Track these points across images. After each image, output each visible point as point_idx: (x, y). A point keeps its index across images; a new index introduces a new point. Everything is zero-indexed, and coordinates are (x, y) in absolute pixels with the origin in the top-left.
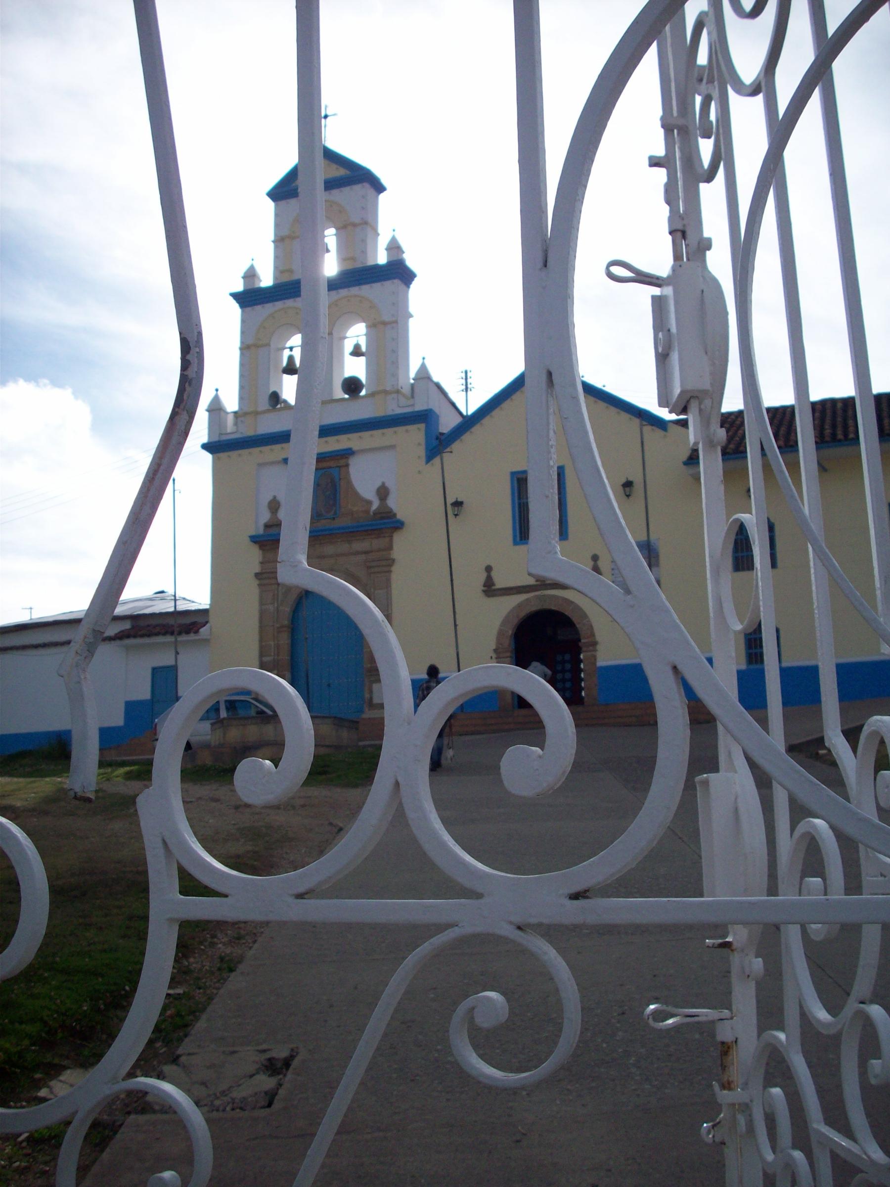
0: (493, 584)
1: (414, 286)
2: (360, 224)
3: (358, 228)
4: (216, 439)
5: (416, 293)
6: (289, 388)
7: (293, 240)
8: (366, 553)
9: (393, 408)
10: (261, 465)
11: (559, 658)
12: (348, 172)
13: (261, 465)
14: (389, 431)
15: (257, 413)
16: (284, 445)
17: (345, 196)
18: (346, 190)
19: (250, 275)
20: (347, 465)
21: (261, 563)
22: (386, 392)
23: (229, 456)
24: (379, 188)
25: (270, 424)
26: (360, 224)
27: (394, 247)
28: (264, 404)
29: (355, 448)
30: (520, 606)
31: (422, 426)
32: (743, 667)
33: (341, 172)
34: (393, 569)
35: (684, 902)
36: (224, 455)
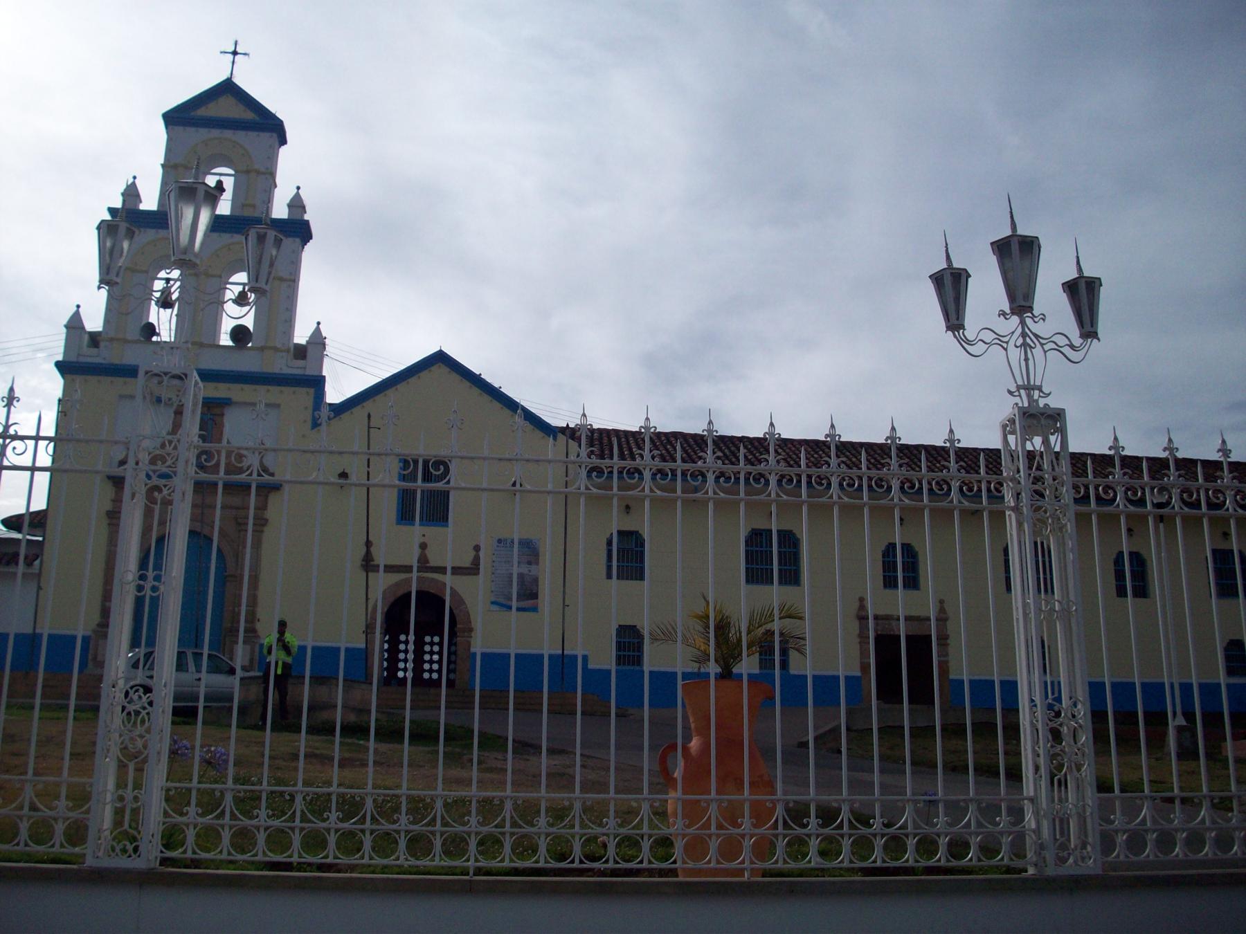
0: (427, 562)
1: (309, 247)
2: (264, 173)
3: (258, 177)
4: (74, 359)
5: (310, 256)
6: (165, 322)
7: (183, 181)
8: (237, 508)
9: (282, 365)
10: (121, 397)
11: (428, 639)
12: (257, 118)
13: (121, 397)
14: (274, 389)
15: (126, 341)
16: (128, 380)
17: (252, 141)
18: (253, 134)
19: (131, 193)
20: (223, 415)
21: (113, 501)
22: (276, 349)
23: (99, 381)
24: (59, 365)
25: (129, 357)
26: (264, 173)
27: (297, 204)
28: (133, 332)
29: (235, 399)
30: (397, 585)
31: (312, 391)
32: (757, 671)
33: (250, 115)
34: (266, 529)
35: (636, 883)
36: (79, 379)
